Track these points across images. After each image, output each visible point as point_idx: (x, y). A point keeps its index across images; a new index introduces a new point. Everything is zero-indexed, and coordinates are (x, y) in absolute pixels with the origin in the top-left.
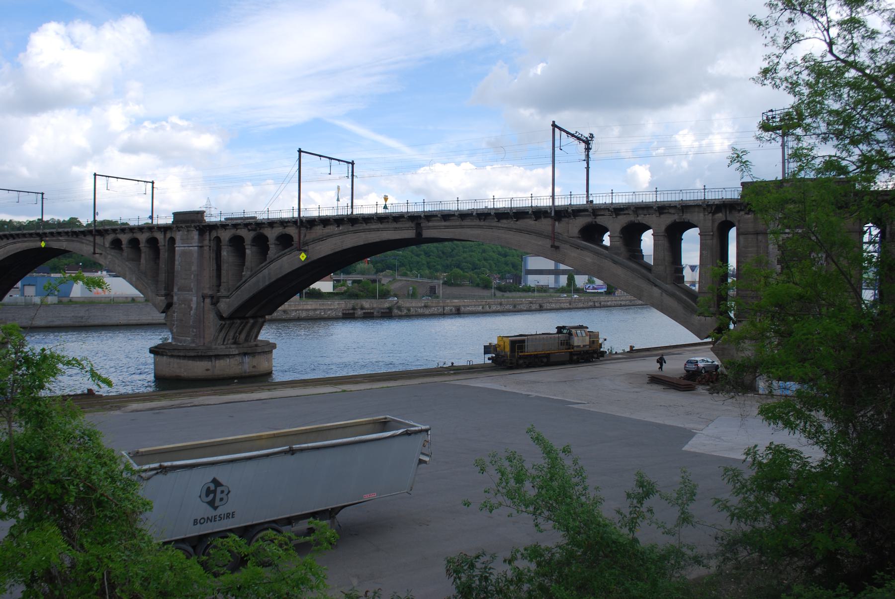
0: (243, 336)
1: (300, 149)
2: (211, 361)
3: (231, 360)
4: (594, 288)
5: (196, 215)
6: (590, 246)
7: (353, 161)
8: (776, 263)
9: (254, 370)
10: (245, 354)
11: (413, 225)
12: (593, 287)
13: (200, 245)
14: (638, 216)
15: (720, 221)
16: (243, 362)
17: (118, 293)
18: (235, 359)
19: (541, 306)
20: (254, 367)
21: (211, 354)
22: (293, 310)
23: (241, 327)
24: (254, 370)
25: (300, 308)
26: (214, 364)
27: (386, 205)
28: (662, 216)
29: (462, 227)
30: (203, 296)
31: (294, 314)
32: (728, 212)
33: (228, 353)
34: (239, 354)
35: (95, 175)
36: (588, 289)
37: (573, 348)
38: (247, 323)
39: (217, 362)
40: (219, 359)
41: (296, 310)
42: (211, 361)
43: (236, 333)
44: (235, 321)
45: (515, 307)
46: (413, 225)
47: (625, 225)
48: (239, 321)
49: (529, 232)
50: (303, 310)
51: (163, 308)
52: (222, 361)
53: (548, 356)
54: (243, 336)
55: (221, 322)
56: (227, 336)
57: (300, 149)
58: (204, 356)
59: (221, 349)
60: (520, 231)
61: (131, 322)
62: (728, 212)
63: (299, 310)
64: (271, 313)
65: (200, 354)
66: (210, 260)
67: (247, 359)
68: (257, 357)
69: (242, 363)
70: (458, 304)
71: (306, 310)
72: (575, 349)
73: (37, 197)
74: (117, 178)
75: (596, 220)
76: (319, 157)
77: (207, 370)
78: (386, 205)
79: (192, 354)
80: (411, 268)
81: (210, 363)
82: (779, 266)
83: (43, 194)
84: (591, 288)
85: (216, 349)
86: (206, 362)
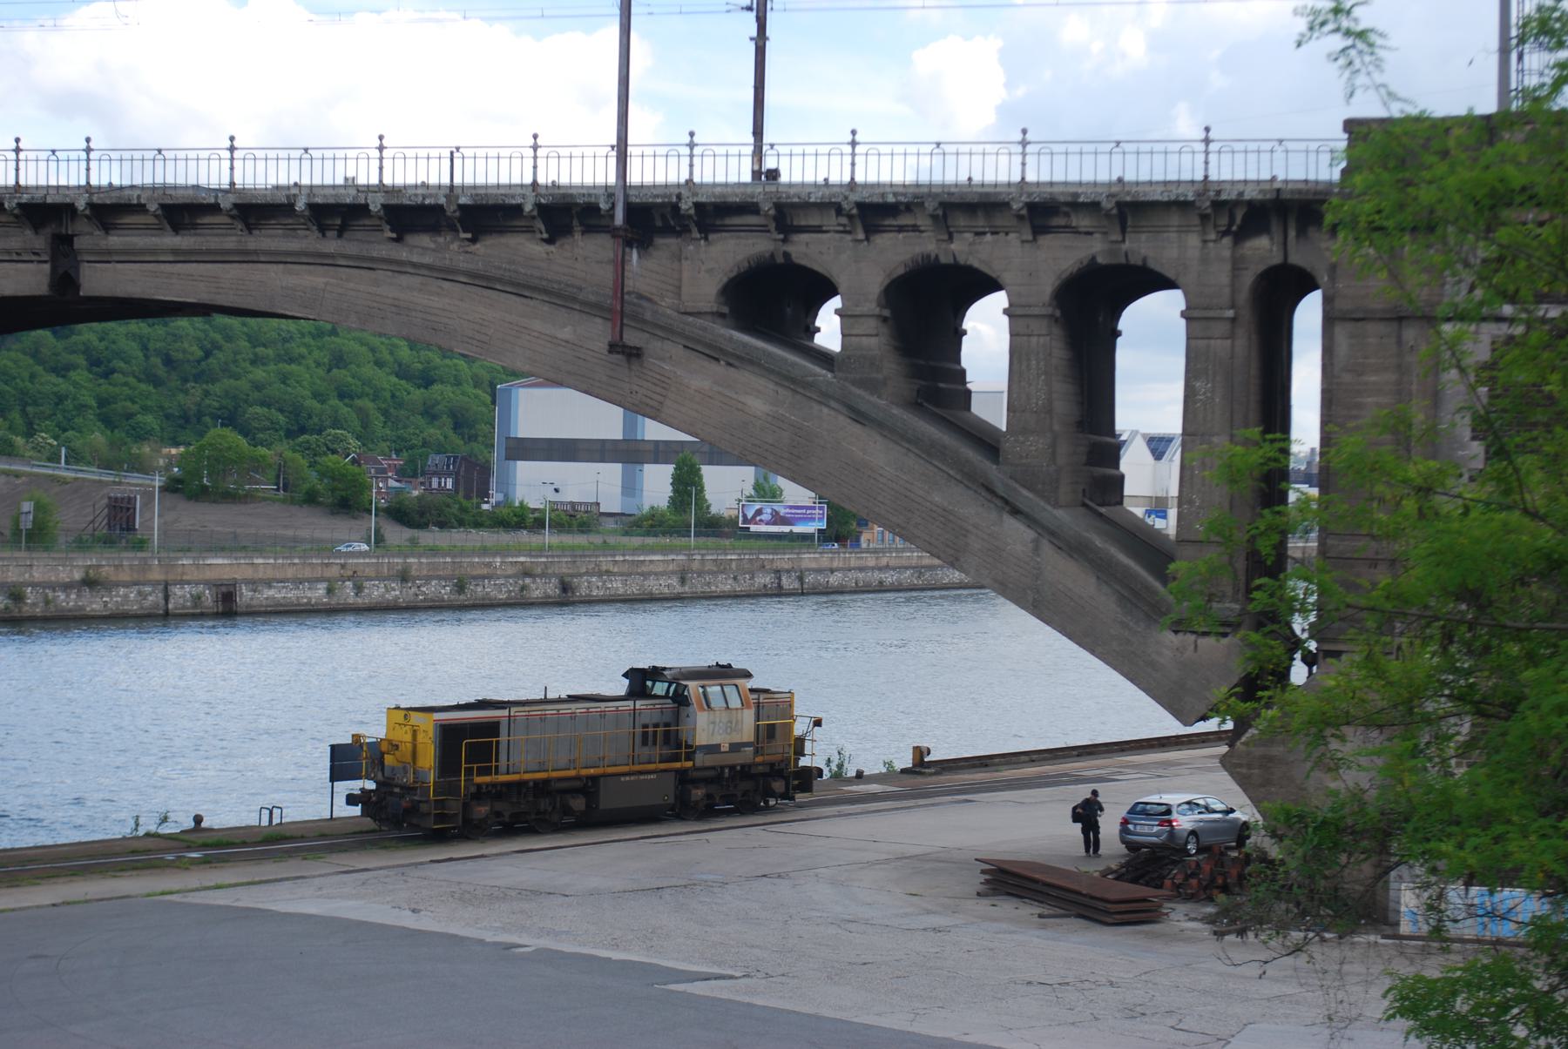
4: (777, 519)
11: (40, 242)
12: (775, 514)
19: (565, 587)
29: (247, 257)
32: (1292, 233)
36: (753, 520)
37: (689, 757)
45: (460, 587)
46: (40, 242)
47: (901, 271)
49: (522, 288)
60: (484, 281)
62: (1292, 233)
70: (227, 575)
72: (701, 759)
75: (789, 248)
84: (766, 517)
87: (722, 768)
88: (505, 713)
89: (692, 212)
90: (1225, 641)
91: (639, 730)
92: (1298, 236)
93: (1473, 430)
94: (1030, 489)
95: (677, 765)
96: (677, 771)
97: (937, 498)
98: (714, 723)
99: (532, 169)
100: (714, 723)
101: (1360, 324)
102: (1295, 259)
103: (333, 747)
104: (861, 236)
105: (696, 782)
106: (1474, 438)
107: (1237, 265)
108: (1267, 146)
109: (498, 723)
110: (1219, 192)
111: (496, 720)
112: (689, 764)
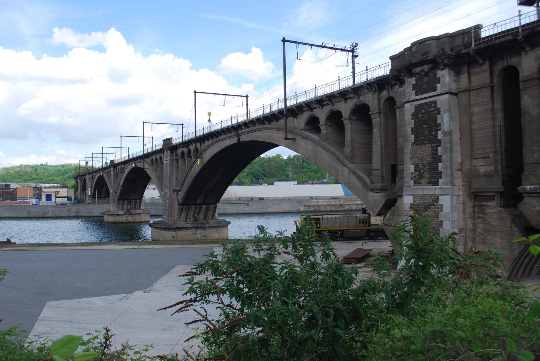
0: (201, 216)
1: (195, 91)
2: (175, 231)
3: (188, 231)
5: (168, 140)
6: (309, 136)
7: (247, 95)
8: (411, 133)
9: (204, 238)
10: (198, 228)
13: (171, 159)
14: (334, 105)
15: (385, 98)
16: (196, 233)
17: (243, 195)
18: (191, 230)
20: (205, 236)
21: (174, 227)
22: (347, 205)
23: (197, 211)
24: (204, 238)
25: (352, 203)
26: (177, 233)
27: (209, 119)
28: (348, 101)
30: (173, 191)
31: (347, 207)
32: (390, 88)
33: (184, 227)
34: (193, 228)
35: (144, 123)
37: (370, 226)
38: (200, 209)
39: (179, 232)
40: (181, 230)
41: (349, 205)
42: (175, 231)
43: (194, 214)
44: (191, 206)
47: (328, 114)
48: (194, 206)
50: (353, 204)
51: (379, 208)
52: (182, 232)
53: (342, 232)
54: (201, 216)
55: (179, 207)
56: (188, 216)
57: (195, 91)
58: (170, 228)
59: (182, 223)
61: (240, 212)
62: (390, 88)
63: (351, 205)
64: (218, 202)
65: (167, 227)
66: (176, 168)
67: (199, 231)
68: (206, 230)
69: (196, 233)
71: (356, 204)
72: (373, 227)
73: (149, 139)
74: (172, 124)
75: (313, 113)
76: (214, 95)
77: (173, 237)
78: (209, 119)
79: (164, 227)
80: (317, 171)
81: (174, 232)
82: (439, 138)
83: (153, 137)
85: (179, 224)
86: (172, 232)
87: (380, 229)
88: (322, 216)
89: (295, 108)
90: (381, 194)
91: (358, 221)
92: (391, 89)
93: (412, 132)
94: (347, 160)
95: (366, 228)
96: (366, 229)
97: (334, 164)
98: (376, 219)
99: (246, 106)
100: (376, 219)
101: (401, 109)
102: (391, 95)
103: (51, 195)
104: (321, 108)
105: (372, 232)
106: (412, 134)
107: (379, 99)
108: (377, 68)
109: (51, 195)
110: (370, 81)
111: (50, 194)
112: (370, 228)
